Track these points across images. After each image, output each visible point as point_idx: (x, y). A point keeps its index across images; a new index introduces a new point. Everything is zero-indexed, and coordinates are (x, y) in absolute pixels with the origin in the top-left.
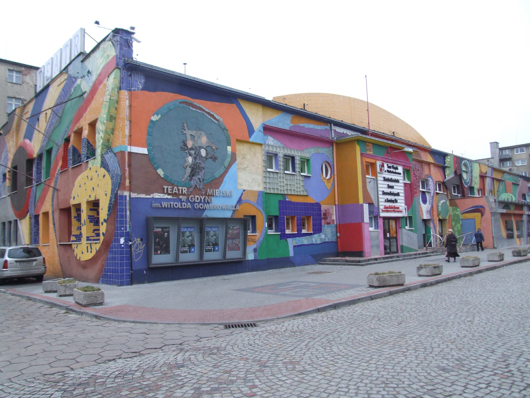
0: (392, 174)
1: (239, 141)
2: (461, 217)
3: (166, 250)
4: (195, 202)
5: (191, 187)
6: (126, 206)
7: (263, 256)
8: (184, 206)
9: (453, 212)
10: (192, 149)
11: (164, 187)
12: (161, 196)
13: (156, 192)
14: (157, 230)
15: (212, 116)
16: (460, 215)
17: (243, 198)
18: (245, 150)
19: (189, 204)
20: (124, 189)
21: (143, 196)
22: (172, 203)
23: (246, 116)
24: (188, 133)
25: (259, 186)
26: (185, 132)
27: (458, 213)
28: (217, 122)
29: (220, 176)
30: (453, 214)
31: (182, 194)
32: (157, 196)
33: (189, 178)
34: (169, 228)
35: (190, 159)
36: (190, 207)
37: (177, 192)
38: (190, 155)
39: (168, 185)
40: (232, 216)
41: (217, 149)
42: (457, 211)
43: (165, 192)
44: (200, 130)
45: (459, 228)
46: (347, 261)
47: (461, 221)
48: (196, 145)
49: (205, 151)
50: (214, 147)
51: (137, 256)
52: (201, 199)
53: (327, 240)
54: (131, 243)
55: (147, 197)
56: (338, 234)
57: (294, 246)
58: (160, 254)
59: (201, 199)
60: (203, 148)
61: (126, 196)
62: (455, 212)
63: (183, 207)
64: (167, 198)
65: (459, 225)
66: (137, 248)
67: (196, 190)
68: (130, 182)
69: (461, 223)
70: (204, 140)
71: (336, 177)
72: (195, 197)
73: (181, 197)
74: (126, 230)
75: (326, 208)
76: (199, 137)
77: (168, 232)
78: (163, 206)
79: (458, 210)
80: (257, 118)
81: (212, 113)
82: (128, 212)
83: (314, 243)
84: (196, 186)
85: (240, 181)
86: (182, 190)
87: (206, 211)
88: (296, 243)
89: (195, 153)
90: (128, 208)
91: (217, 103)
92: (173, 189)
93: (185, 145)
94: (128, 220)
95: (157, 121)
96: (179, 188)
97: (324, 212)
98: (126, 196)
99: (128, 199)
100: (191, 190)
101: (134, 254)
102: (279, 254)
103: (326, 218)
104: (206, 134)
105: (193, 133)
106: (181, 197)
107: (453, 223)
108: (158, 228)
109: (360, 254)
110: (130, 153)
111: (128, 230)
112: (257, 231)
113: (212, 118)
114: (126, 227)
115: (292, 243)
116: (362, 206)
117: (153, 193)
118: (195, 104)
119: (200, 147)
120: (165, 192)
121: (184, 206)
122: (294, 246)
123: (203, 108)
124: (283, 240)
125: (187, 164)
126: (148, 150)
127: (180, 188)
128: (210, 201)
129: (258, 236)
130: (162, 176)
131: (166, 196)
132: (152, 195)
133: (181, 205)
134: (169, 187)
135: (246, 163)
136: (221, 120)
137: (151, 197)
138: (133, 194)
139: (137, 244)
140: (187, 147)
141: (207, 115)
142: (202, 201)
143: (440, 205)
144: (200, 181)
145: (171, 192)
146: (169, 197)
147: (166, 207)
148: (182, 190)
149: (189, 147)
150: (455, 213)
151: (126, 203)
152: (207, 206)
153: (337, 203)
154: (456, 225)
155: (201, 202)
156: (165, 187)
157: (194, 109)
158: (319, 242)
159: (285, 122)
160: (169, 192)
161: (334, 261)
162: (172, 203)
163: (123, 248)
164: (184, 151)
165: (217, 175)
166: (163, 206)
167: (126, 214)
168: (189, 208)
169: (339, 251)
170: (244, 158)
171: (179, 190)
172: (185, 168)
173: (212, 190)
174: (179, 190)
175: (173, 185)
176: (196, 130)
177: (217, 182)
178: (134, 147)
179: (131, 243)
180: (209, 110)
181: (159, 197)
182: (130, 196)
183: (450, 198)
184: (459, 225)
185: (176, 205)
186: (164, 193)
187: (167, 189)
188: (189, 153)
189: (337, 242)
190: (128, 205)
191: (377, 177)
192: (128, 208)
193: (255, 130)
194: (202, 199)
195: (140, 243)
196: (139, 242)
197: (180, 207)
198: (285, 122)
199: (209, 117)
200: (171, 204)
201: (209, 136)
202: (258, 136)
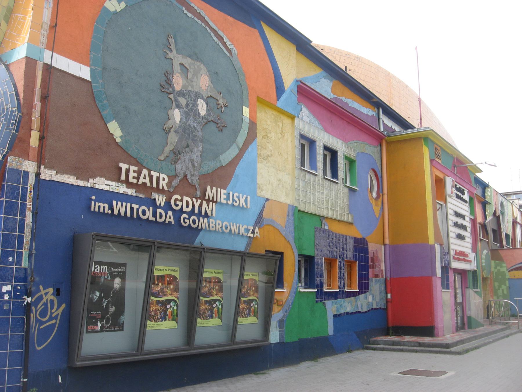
0: (459, 200)
1: (262, 102)
2: (508, 275)
3: (116, 324)
4: (181, 211)
5: (176, 176)
6: (24, 198)
7: (292, 338)
8: (161, 217)
9: (496, 268)
10: (181, 94)
11: (121, 165)
12: (113, 186)
13: (102, 176)
14: (97, 270)
15: (221, 39)
16: (507, 272)
17: (265, 215)
18: (269, 123)
19: (170, 213)
20: (25, 154)
21: (71, 180)
22: (135, 206)
23: (274, 58)
24: (178, 59)
25: (287, 195)
26: (171, 55)
27: (504, 269)
28: (228, 54)
29: (230, 163)
30: (496, 270)
31: (158, 190)
32: (102, 184)
33: (172, 156)
34: (124, 265)
35: (177, 115)
36: (172, 220)
37: (147, 181)
38: (178, 106)
39: (130, 164)
40: (246, 248)
41: (226, 106)
42: (501, 267)
43: (123, 177)
44: (198, 59)
45: (505, 292)
46: (420, 345)
47: (507, 282)
48: (190, 88)
49: (204, 104)
50: (221, 102)
51: (44, 334)
52: (194, 206)
53: (375, 306)
54: (29, 300)
55: (81, 183)
56: (389, 296)
57: (335, 316)
58: (102, 330)
59: (194, 206)
60: (202, 98)
61: (26, 174)
62: (498, 268)
63: (158, 220)
64: (124, 195)
65: (504, 287)
66: (43, 313)
67: (185, 186)
68: (42, 139)
69: (507, 284)
70: (204, 83)
71: (386, 197)
72: (182, 200)
73: (155, 195)
74: (19, 262)
75: (374, 250)
76: (196, 74)
77: (123, 277)
78: (116, 212)
79: (504, 265)
80: (292, 68)
81: (220, 33)
82: (29, 217)
83: (360, 310)
84: (185, 176)
85: (260, 180)
86: (158, 178)
87: (201, 234)
88: (338, 310)
89: (187, 105)
90: (29, 203)
91: (229, 18)
92: (139, 173)
93: (169, 83)
94: (27, 235)
95: (115, 13)
96: (153, 173)
97: (372, 256)
98: (26, 174)
99: (32, 180)
100: (175, 182)
101: (35, 330)
102: (311, 332)
103: (373, 267)
104: (209, 71)
105: (187, 62)
106: (155, 195)
107: (496, 284)
108: (100, 263)
109: (429, 330)
110: (49, 69)
111: (25, 264)
112: (286, 284)
113: (219, 43)
114: (20, 254)
115: (332, 307)
116: (433, 248)
117: (94, 177)
118: (193, 5)
119: (198, 95)
120: (123, 177)
121: (161, 217)
122: (335, 316)
123: (207, 18)
124: (320, 304)
125: (170, 124)
126: (92, 72)
127: (155, 174)
128: (209, 213)
129: (286, 295)
130: (118, 140)
131: (123, 189)
132: (91, 180)
133: (154, 215)
134: (133, 168)
135: (269, 146)
136: (235, 51)
137: (89, 185)
138: (47, 171)
139: (45, 304)
140: (173, 88)
141: (212, 35)
142: (196, 211)
143: (484, 257)
144: (193, 165)
145: (135, 181)
146: (130, 192)
147: (122, 213)
148: (158, 178)
149: (178, 87)
150: (499, 270)
151: (25, 190)
152: (204, 223)
153: (387, 241)
154: (500, 287)
155: (192, 212)
156: (124, 166)
157: (189, 15)
158: (365, 310)
159: (325, 87)
160: (131, 180)
161: (394, 343)
162: (135, 206)
163: (7, 313)
164: (165, 95)
165: (226, 158)
166: (116, 212)
167: (22, 222)
168: (170, 222)
169: (390, 325)
170: (266, 136)
171: (151, 177)
172: (167, 132)
173: (214, 189)
174: (151, 177)
175: (141, 166)
176: (190, 56)
177: (222, 176)
178: (60, 57)
179: (29, 300)
180: (216, 25)
181: (107, 188)
182: (38, 174)
183: (491, 248)
184: (504, 287)
185: (144, 212)
186: (118, 179)
187: (128, 171)
188: (176, 100)
189: (386, 310)
190: (29, 197)
191: (446, 202)
192: (29, 203)
193: (286, 87)
194: (197, 205)
195: (52, 301)
196: (50, 297)
197: (152, 219)
198: (325, 87)
199: (216, 40)
200: (132, 209)
201: (214, 76)
202: (289, 99)
